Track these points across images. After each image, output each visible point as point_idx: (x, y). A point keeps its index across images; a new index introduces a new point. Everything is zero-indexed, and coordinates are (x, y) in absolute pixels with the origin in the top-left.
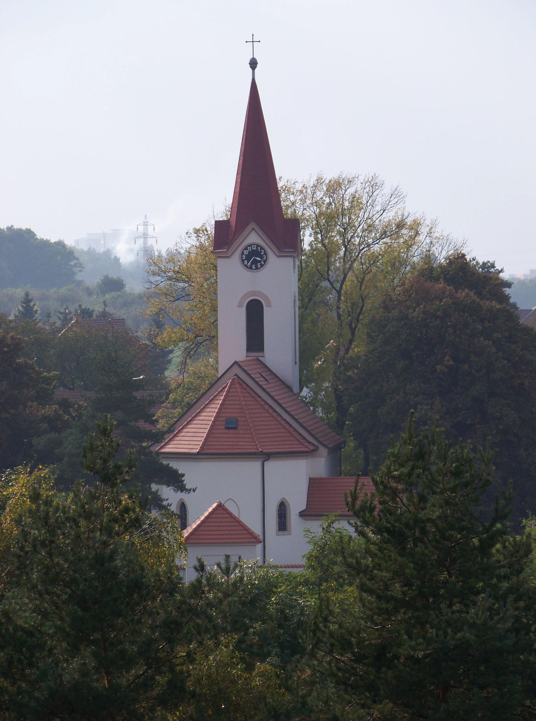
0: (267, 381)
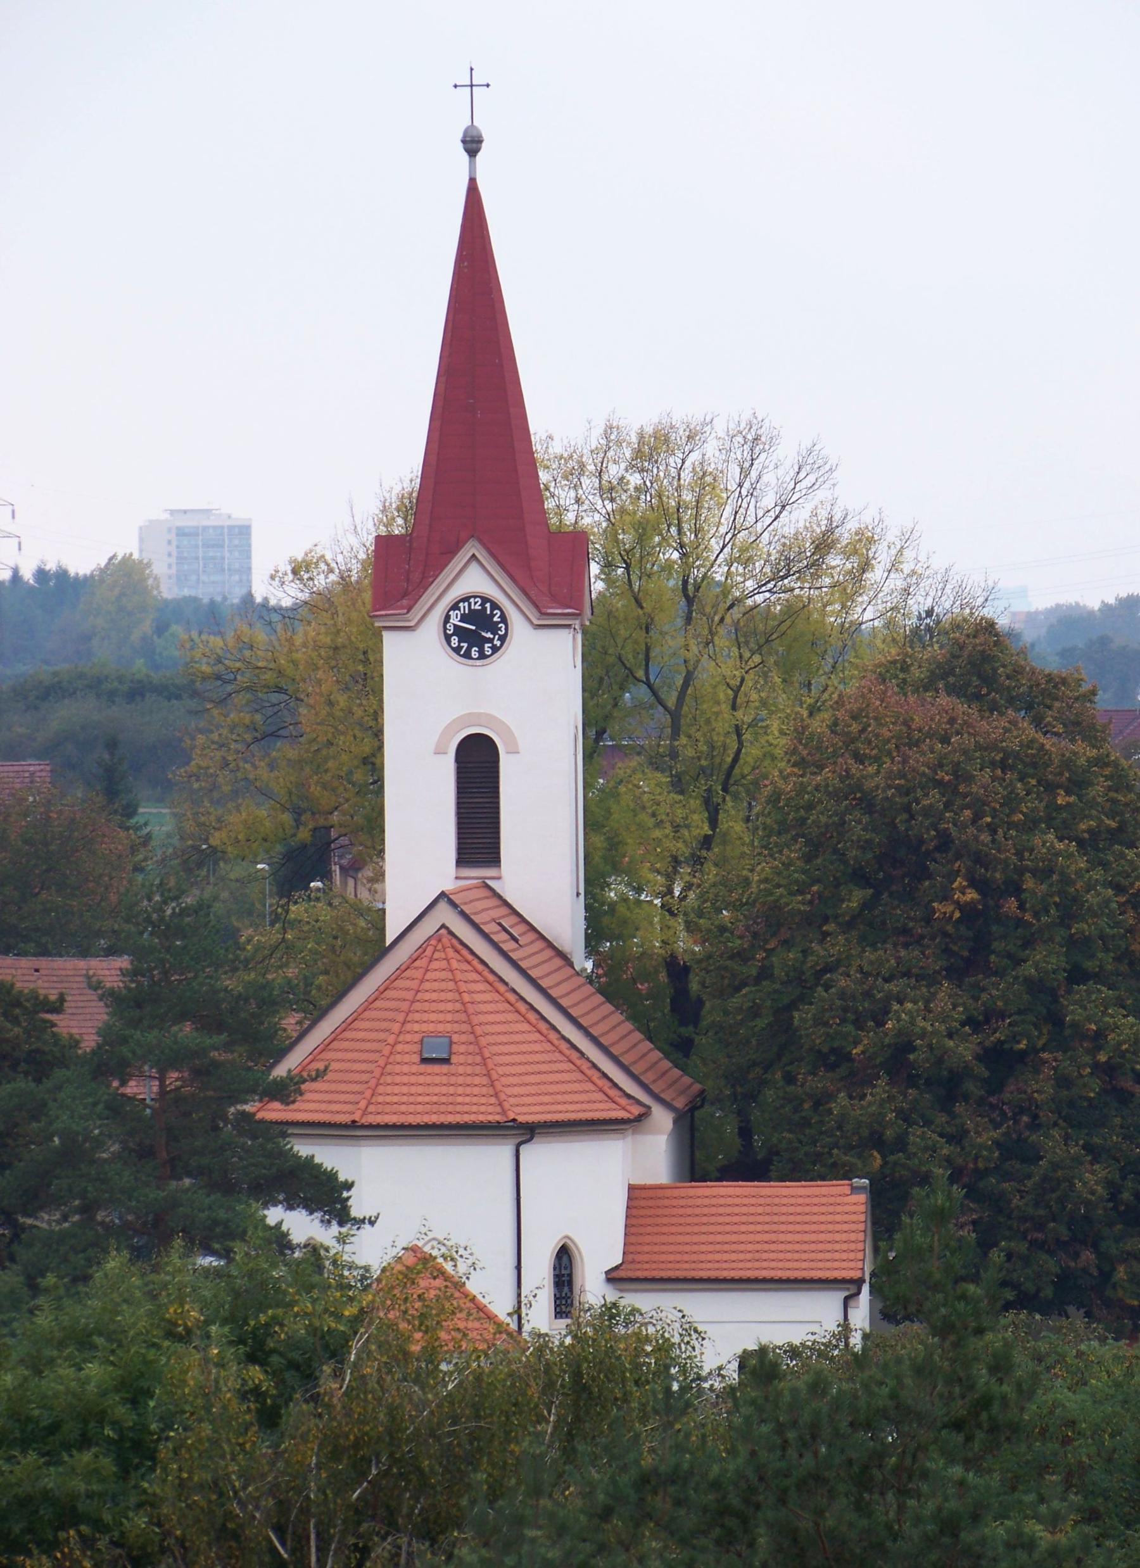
0: (516, 941)
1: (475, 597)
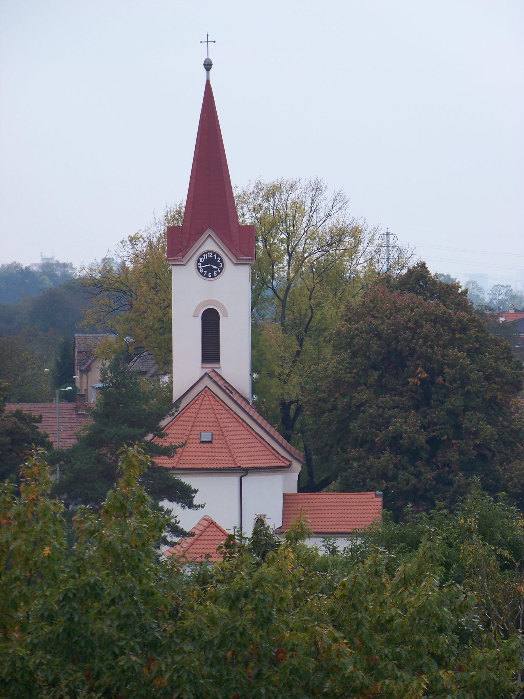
1: (210, 252)
